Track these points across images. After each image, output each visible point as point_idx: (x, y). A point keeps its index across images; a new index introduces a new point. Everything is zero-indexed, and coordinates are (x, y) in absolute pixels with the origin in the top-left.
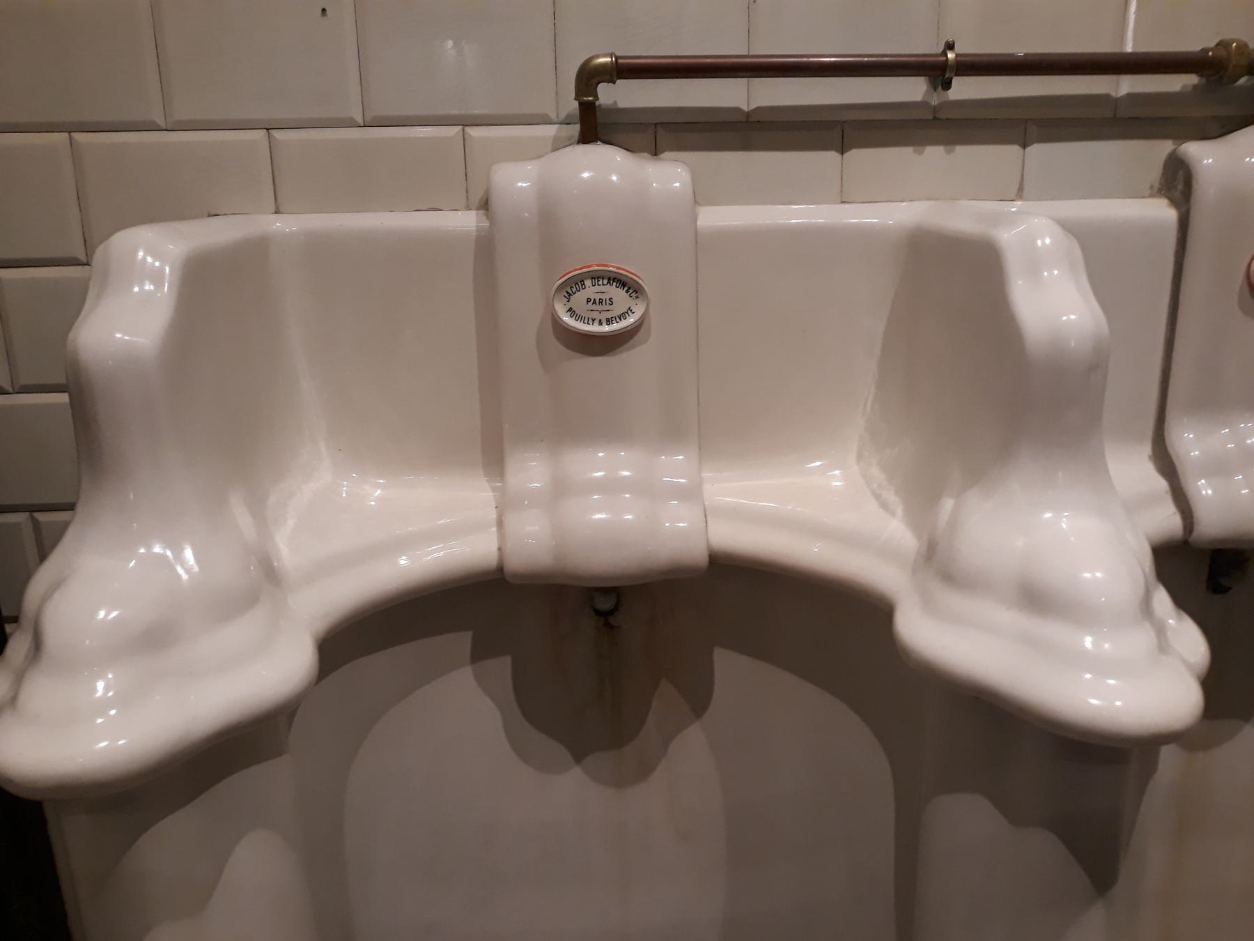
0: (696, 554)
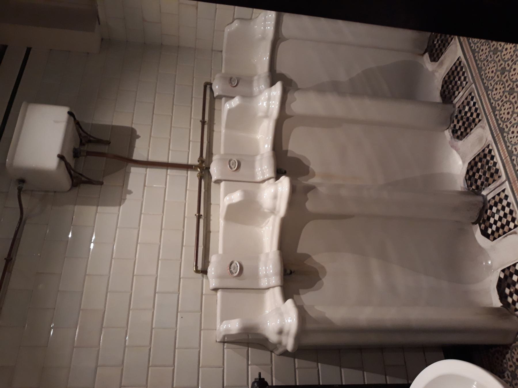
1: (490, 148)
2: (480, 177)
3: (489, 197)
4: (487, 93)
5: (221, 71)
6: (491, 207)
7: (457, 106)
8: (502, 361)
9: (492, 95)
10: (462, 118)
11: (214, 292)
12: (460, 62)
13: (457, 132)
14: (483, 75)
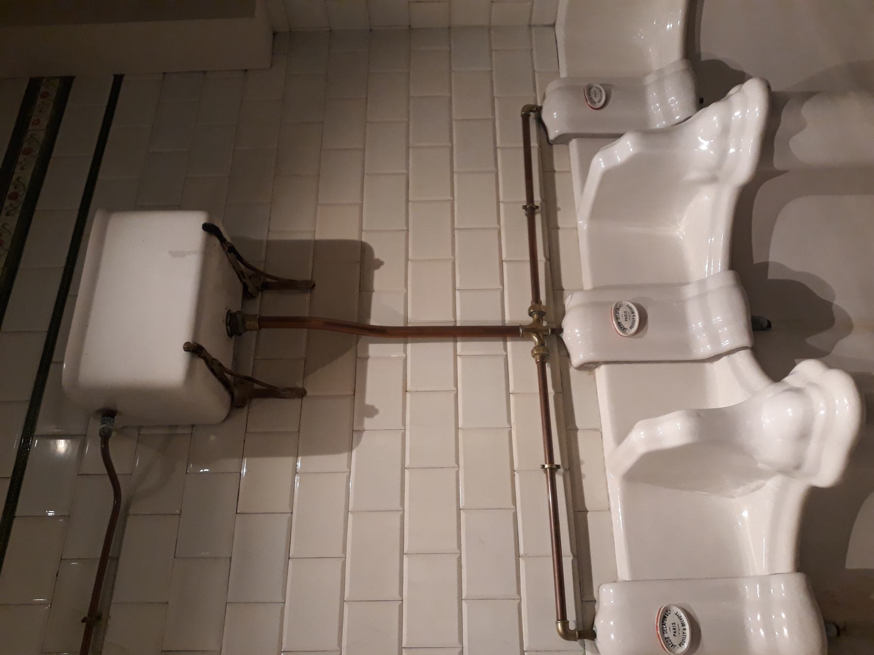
0: (797, 581)
5: (558, 73)
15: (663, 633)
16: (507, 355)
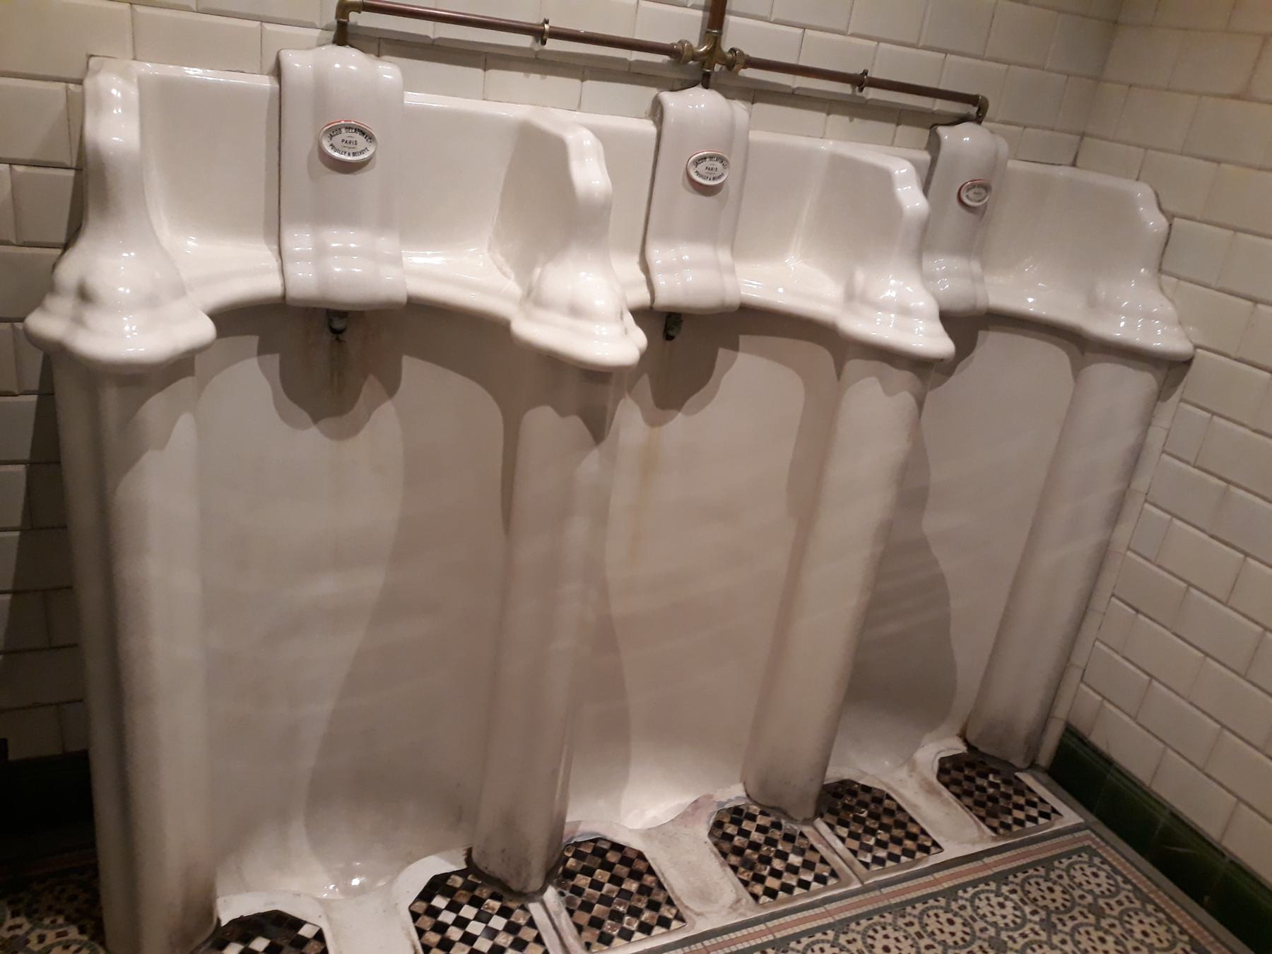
0: (401, 296)
1: (675, 924)
2: (597, 885)
3: (535, 909)
4: (830, 926)
5: (1015, 158)
6: (505, 912)
7: (807, 830)
8: (59, 912)
9: (823, 941)
10: (771, 842)
11: (271, 62)
12: (926, 850)
13: (733, 822)
14: (882, 920)
15: (346, 128)
16: (686, 7)
